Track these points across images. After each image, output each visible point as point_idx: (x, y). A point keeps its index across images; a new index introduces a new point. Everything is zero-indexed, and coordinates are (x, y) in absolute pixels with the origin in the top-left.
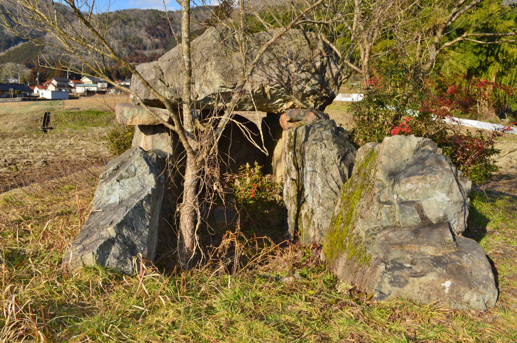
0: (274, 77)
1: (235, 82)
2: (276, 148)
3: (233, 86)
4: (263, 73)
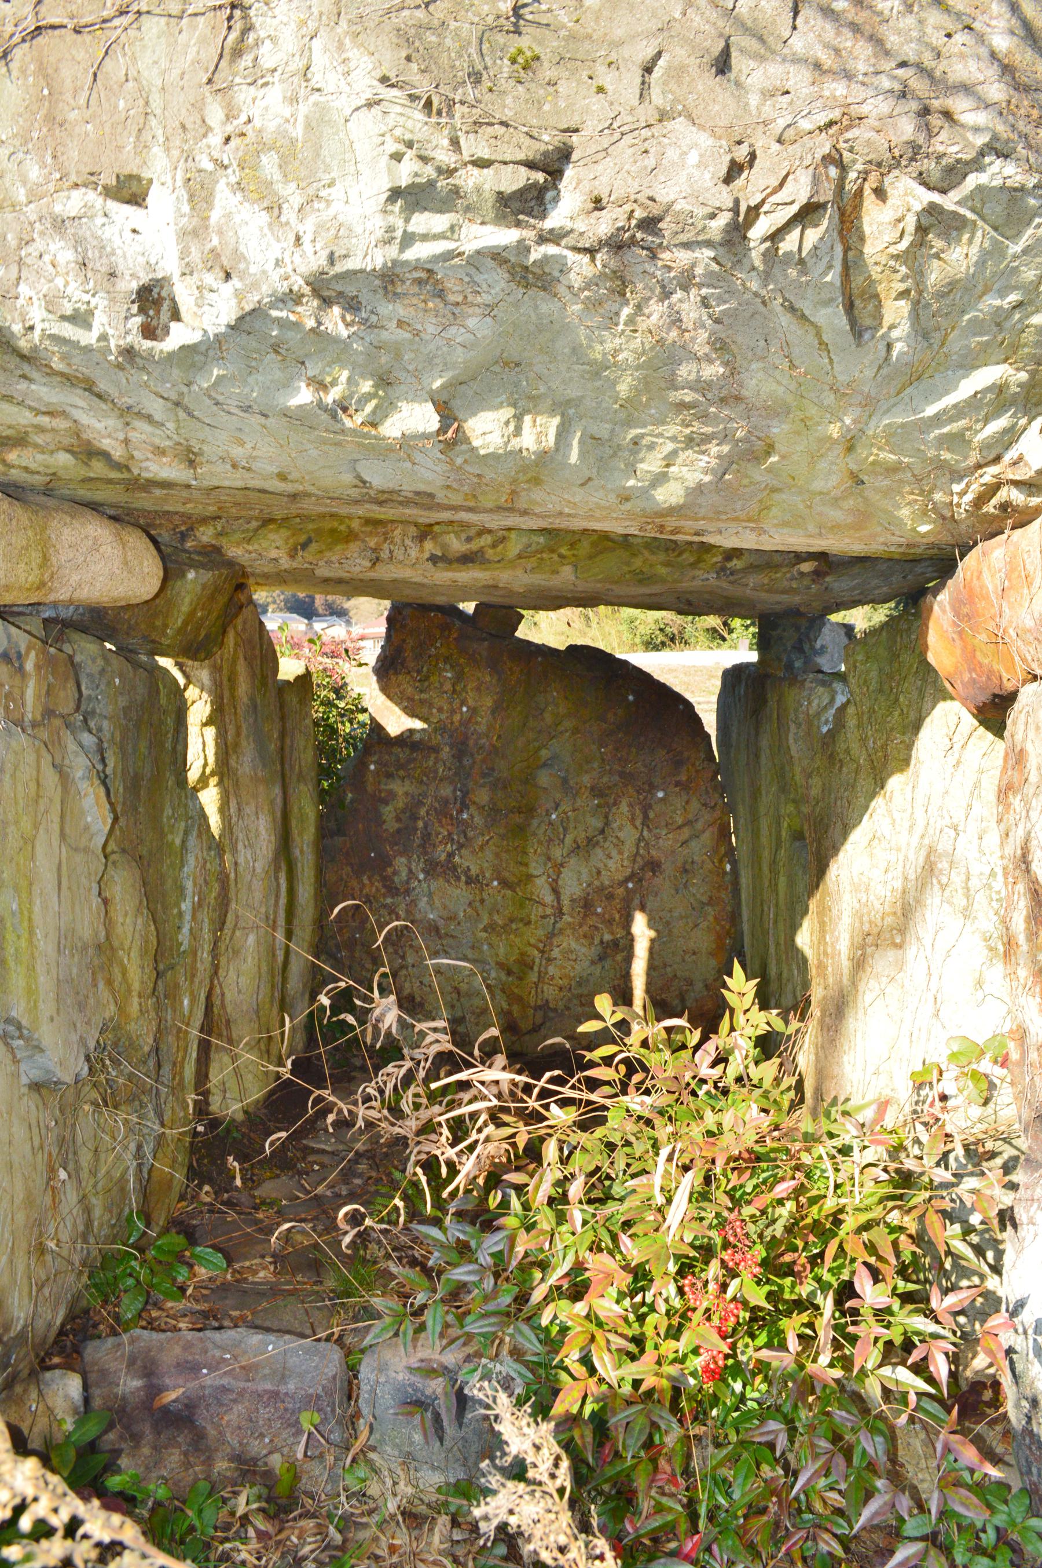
0: (966, 88)
1: (549, 140)
2: (858, 837)
3: (518, 179)
4: (847, 40)
